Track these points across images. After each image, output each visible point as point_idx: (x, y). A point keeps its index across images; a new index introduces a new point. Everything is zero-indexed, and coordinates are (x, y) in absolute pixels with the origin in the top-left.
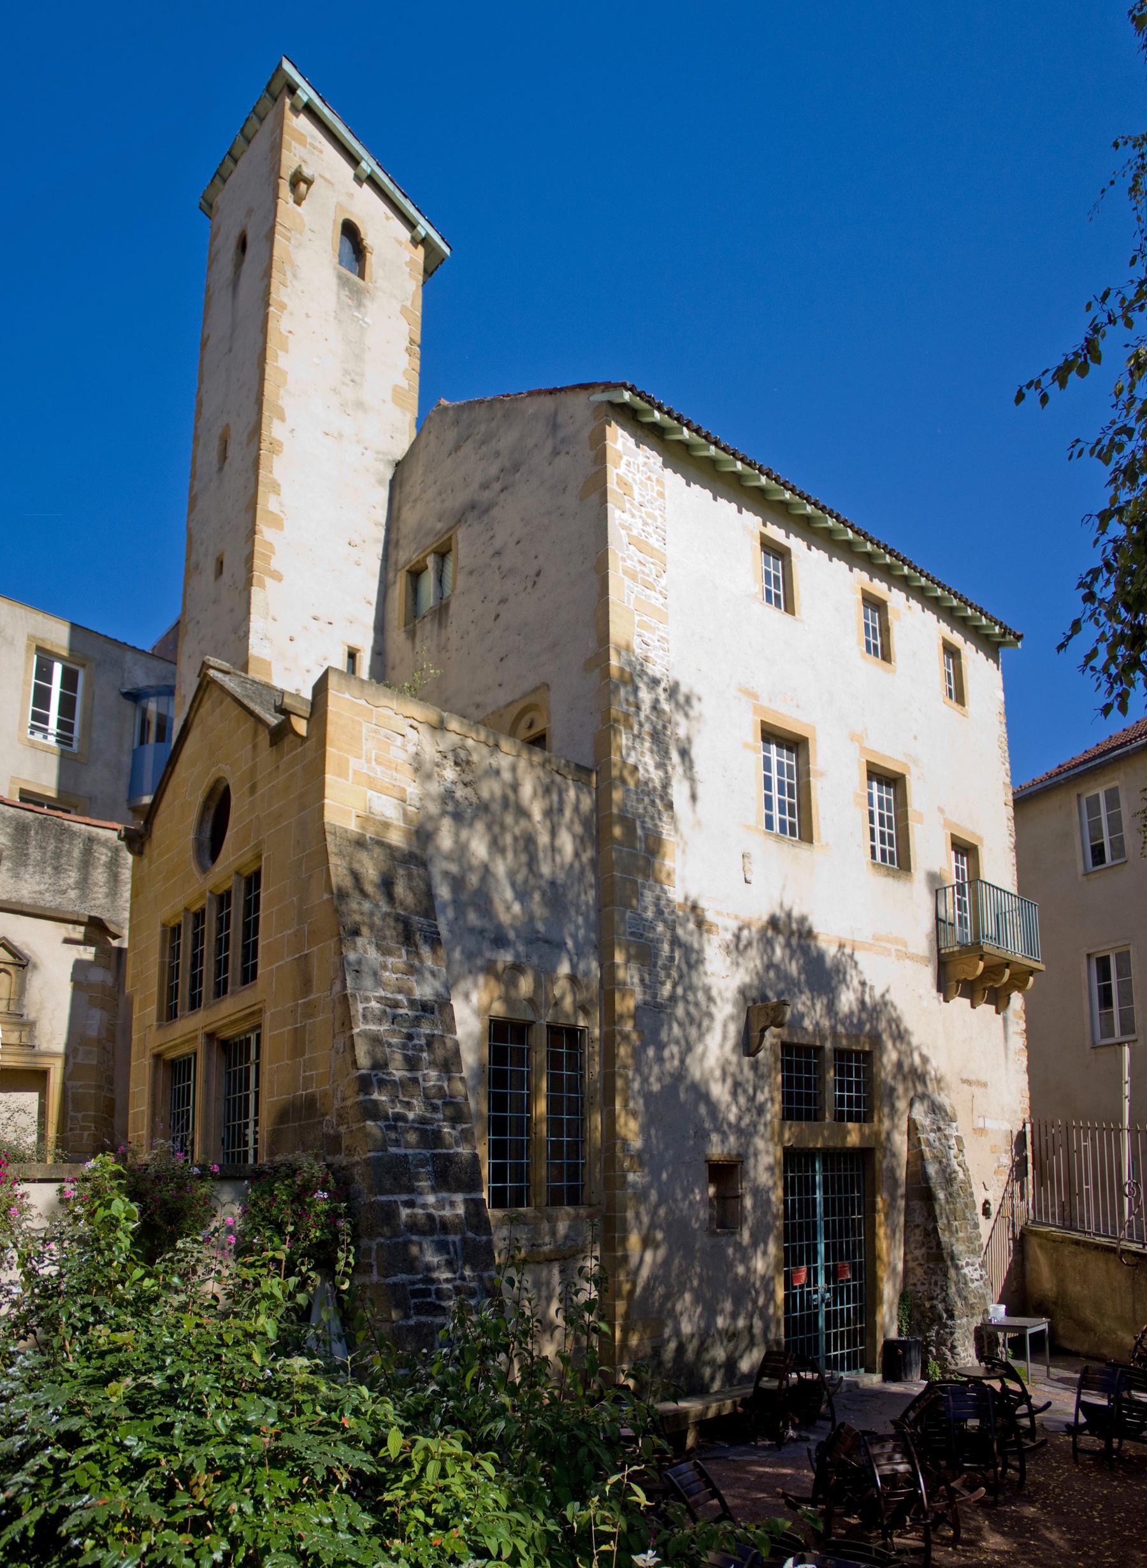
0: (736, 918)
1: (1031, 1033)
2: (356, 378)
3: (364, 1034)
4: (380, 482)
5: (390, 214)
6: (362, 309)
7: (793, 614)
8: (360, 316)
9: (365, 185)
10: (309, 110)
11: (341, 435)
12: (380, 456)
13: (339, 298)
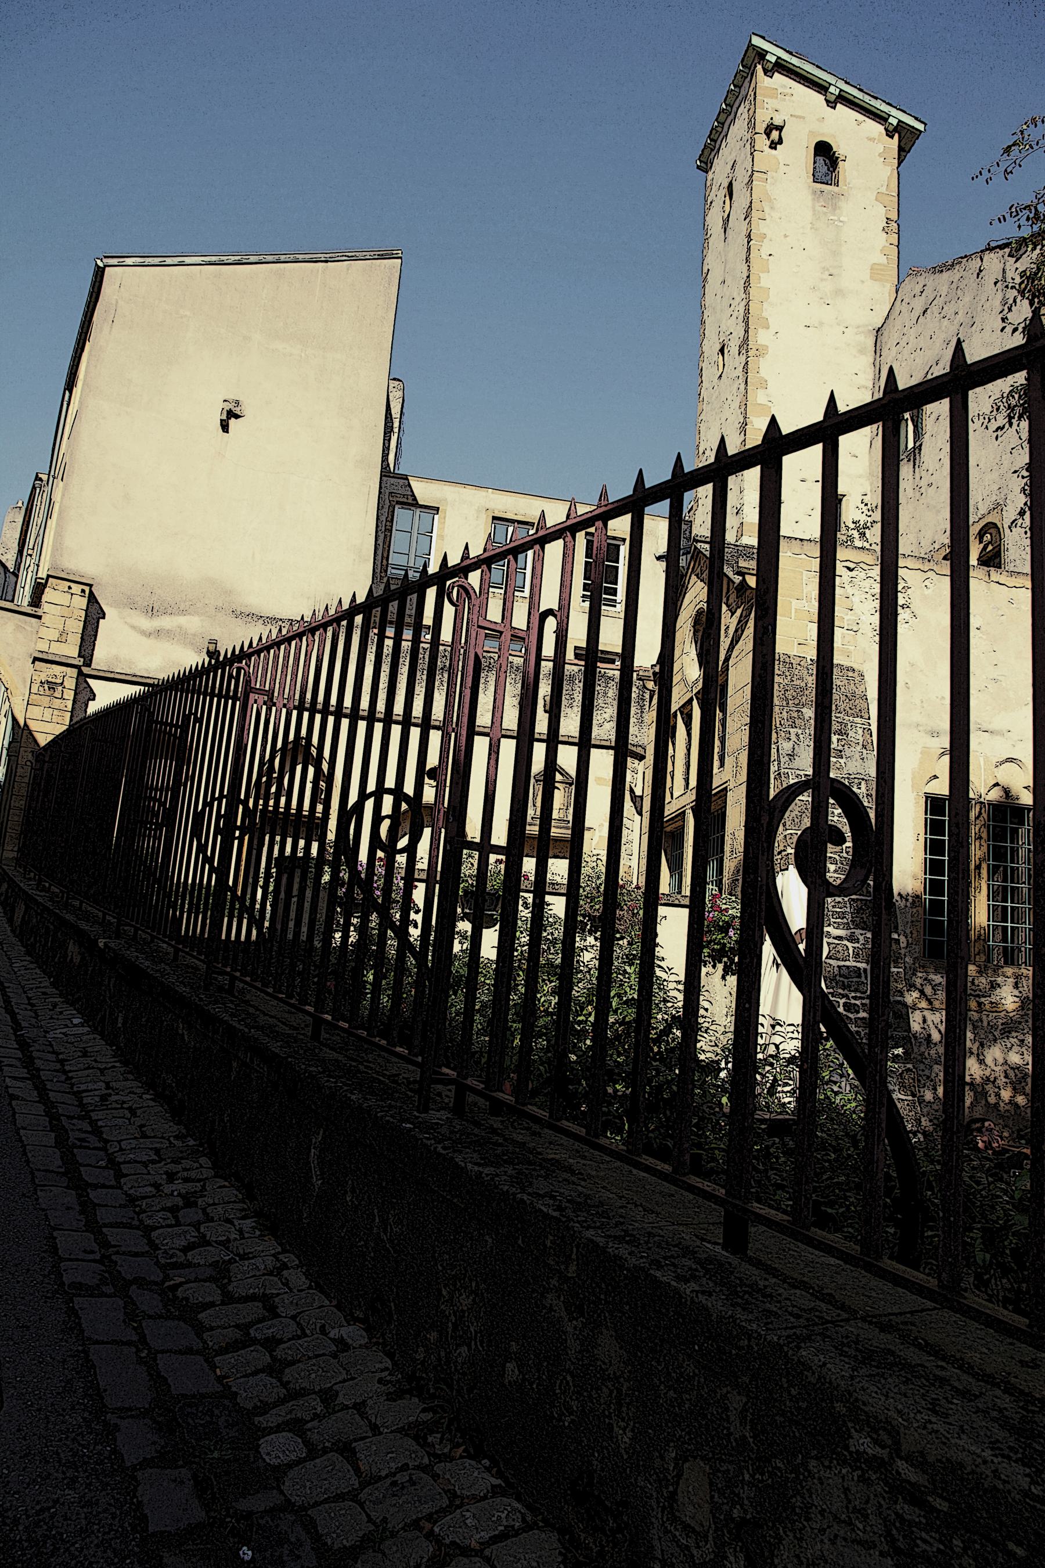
0: (943, 754)
1: (892, 889)
2: (832, 271)
3: (1024, 903)
4: (862, 351)
5: (861, 117)
6: (838, 211)
7: (227, 432)
8: (836, 218)
9: (839, 106)
10: (781, 67)
11: (821, 324)
12: (860, 330)
13: (814, 210)
